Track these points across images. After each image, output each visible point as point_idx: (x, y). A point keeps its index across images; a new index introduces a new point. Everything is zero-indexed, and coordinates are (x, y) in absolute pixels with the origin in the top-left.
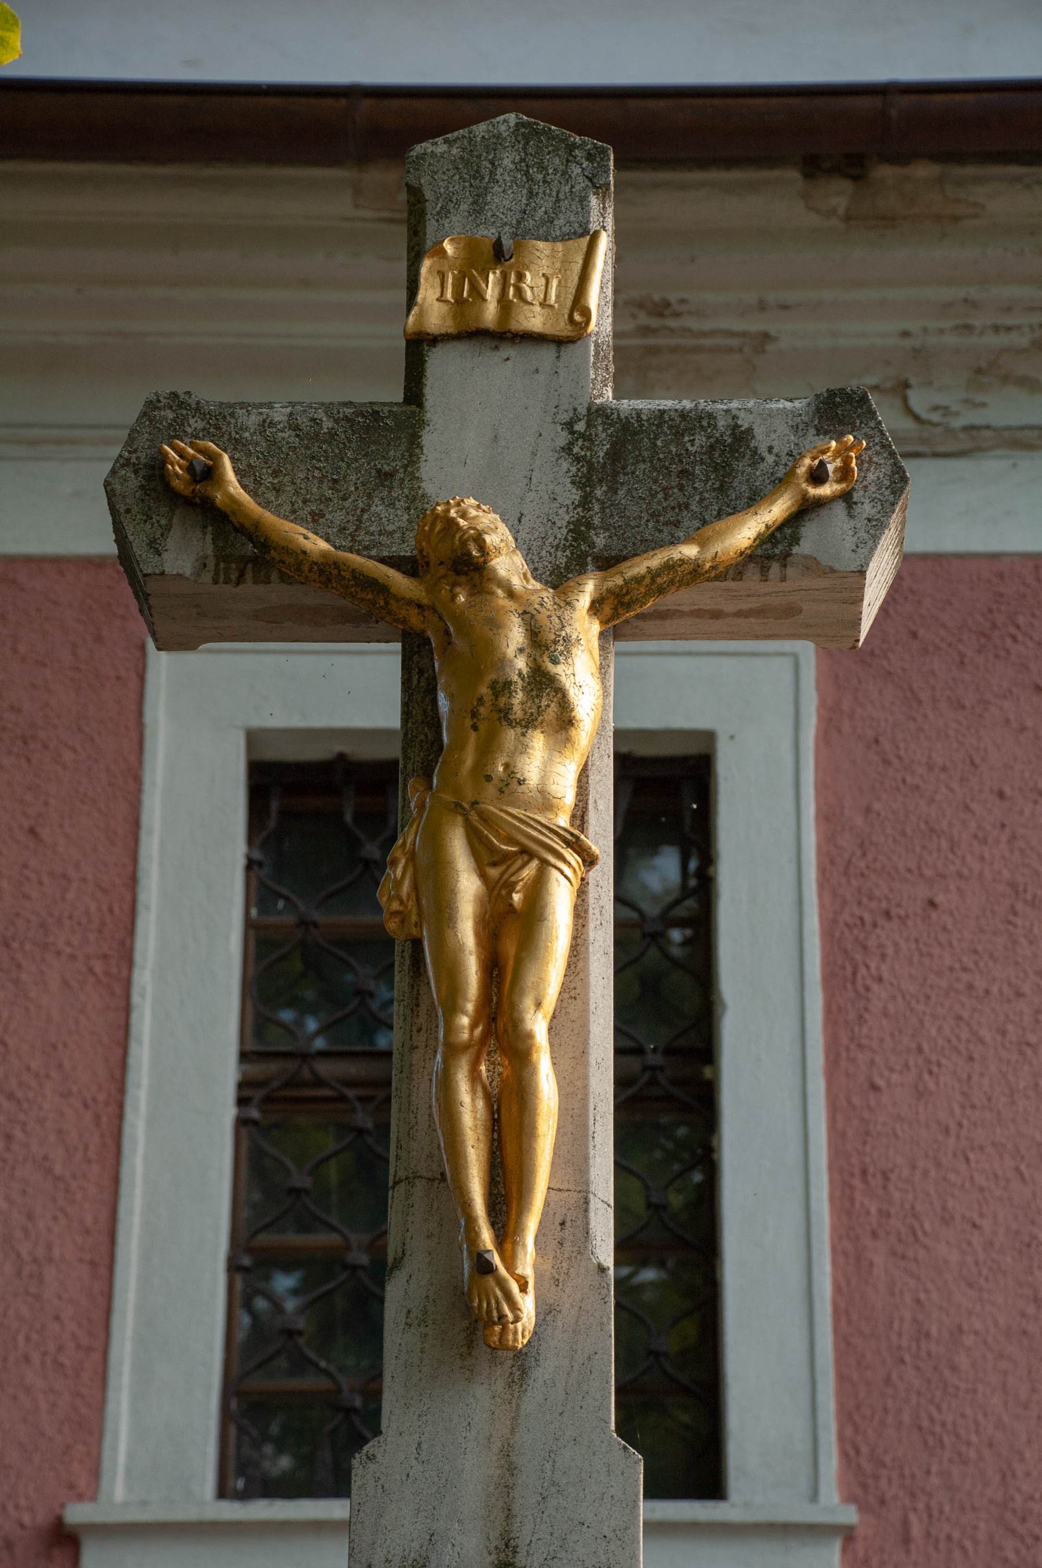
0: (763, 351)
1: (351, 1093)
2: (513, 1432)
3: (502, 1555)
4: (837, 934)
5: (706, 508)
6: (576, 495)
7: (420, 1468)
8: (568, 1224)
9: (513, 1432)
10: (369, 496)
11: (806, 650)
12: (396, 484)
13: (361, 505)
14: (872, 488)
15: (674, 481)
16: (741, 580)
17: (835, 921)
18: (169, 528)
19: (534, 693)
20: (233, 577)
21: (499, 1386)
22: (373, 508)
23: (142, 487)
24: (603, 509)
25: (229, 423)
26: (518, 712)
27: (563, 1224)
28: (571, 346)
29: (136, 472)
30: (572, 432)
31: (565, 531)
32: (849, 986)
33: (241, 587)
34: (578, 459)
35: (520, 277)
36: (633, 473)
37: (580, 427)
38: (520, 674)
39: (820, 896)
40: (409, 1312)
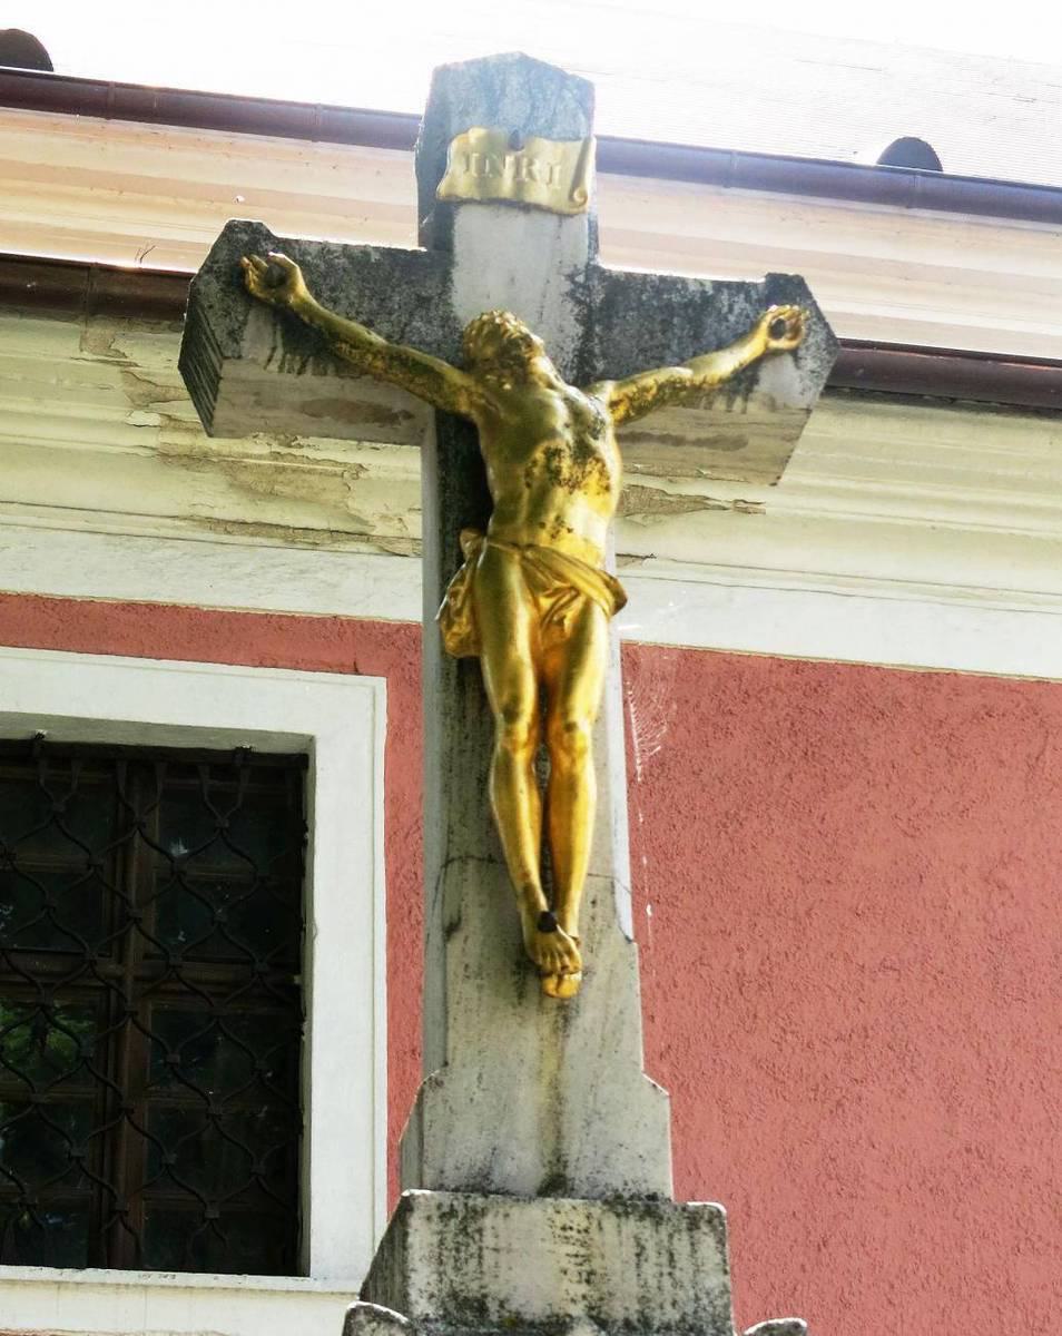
0: (358, 478)
1: (38, 980)
2: (559, 1068)
3: (555, 1168)
4: (398, 884)
5: (684, 349)
6: (580, 330)
7: (481, 1094)
8: (599, 902)
9: (559, 1068)
10: (411, 314)
11: (380, 684)
12: (432, 307)
13: (404, 320)
14: (813, 348)
15: (658, 327)
16: (710, 409)
17: (397, 874)
18: (245, 323)
19: (579, 460)
20: (297, 367)
21: (546, 1031)
22: (414, 323)
23: (222, 289)
24: (601, 343)
25: (294, 249)
26: (565, 473)
27: (594, 902)
28: (571, 220)
29: (217, 278)
30: (573, 282)
31: (571, 356)
32: (406, 920)
33: (301, 377)
34: (579, 302)
35: (531, 163)
36: (624, 317)
37: (580, 279)
38: (568, 445)
39: (386, 856)
40: (467, 966)
